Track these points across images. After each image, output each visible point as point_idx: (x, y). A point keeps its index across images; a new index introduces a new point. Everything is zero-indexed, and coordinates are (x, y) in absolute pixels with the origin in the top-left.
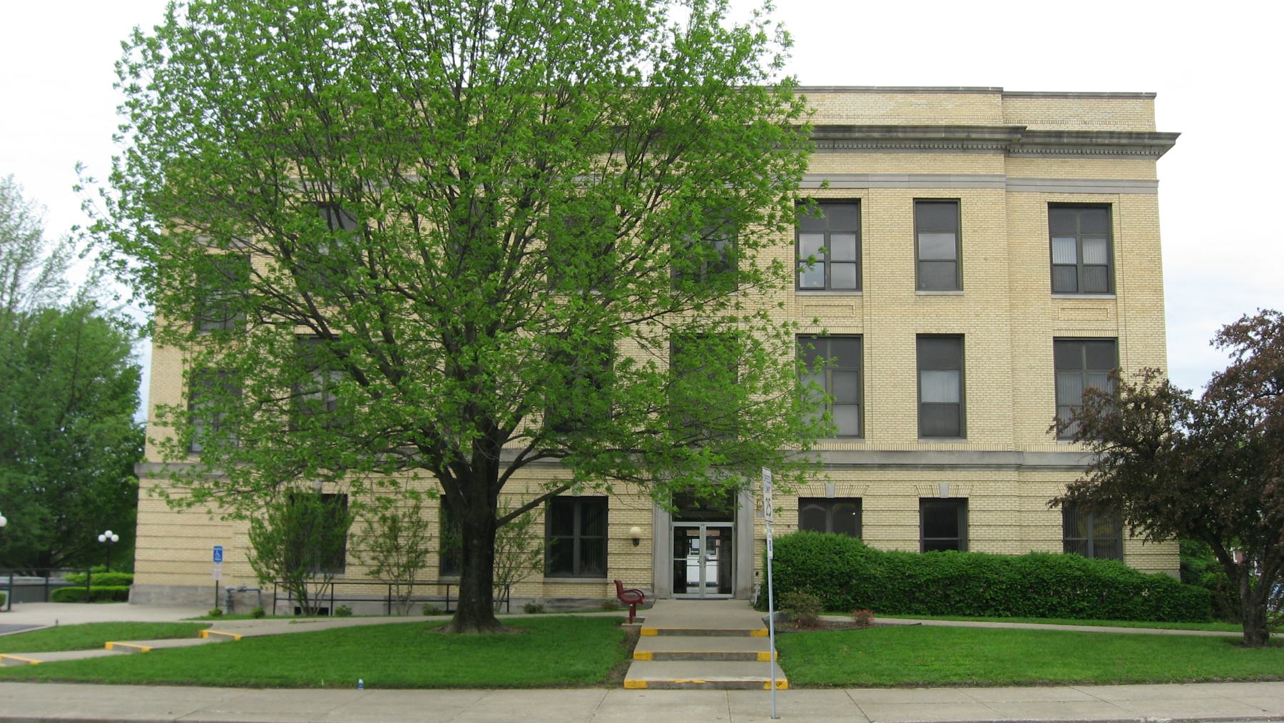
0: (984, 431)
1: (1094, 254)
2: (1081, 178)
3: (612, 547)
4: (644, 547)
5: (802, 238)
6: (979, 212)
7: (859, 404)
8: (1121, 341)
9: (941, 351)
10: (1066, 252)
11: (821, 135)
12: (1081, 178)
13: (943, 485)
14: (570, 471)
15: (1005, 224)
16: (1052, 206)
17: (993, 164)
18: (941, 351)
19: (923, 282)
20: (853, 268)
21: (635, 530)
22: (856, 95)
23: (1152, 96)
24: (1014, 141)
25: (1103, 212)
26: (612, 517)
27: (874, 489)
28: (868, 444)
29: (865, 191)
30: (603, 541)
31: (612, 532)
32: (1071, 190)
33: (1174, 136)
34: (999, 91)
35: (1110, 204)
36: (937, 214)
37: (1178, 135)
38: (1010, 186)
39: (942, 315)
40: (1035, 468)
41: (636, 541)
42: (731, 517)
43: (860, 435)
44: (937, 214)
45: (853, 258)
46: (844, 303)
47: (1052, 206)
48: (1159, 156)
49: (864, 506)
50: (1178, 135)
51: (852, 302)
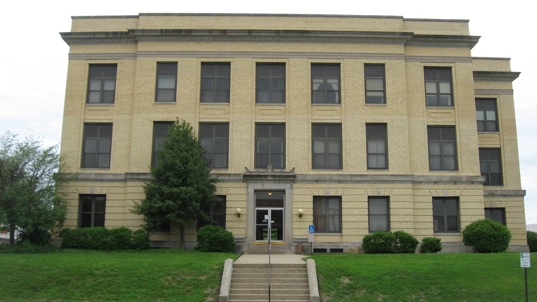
0: (118, 164)
1: (445, 88)
2: (437, 55)
3: (228, 218)
4: (243, 218)
5: (368, 81)
6: (395, 71)
7: (314, 155)
8: (457, 127)
9: (377, 131)
10: (432, 88)
11: (401, 36)
12: (437, 55)
13: (382, 190)
14: (410, 185)
15: (405, 77)
16: (425, 68)
17: (399, 49)
18: (377, 131)
19: (369, 100)
20: (91, 89)
21: (239, 210)
22: (249, 17)
23: (467, 21)
24: (250, 35)
25: (448, 70)
26: (228, 204)
27: (395, 192)
28: (391, 172)
29: (288, 60)
30: (224, 215)
31: (228, 211)
32: (215, 56)
33: (478, 38)
34: (401, 18)
35: (451, 67)
36: (375, 71)
37: (480, 37)
38: (407, 59)
39: (376, 115)
40: (420, 182)
41: (239, 215)
42: (281, 203)
43: (386, 167)
44: (375, 71)
45: (382, 89)
46: (277, 108)
47: (425, 68)
48: (472, 47)
49: (391, 200)
50: (480, 37)
51: (336, 108)
